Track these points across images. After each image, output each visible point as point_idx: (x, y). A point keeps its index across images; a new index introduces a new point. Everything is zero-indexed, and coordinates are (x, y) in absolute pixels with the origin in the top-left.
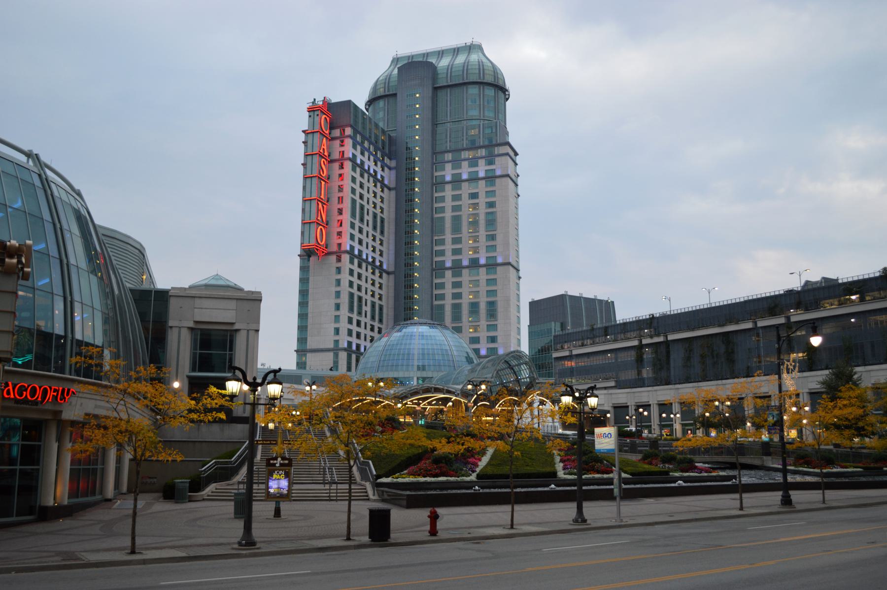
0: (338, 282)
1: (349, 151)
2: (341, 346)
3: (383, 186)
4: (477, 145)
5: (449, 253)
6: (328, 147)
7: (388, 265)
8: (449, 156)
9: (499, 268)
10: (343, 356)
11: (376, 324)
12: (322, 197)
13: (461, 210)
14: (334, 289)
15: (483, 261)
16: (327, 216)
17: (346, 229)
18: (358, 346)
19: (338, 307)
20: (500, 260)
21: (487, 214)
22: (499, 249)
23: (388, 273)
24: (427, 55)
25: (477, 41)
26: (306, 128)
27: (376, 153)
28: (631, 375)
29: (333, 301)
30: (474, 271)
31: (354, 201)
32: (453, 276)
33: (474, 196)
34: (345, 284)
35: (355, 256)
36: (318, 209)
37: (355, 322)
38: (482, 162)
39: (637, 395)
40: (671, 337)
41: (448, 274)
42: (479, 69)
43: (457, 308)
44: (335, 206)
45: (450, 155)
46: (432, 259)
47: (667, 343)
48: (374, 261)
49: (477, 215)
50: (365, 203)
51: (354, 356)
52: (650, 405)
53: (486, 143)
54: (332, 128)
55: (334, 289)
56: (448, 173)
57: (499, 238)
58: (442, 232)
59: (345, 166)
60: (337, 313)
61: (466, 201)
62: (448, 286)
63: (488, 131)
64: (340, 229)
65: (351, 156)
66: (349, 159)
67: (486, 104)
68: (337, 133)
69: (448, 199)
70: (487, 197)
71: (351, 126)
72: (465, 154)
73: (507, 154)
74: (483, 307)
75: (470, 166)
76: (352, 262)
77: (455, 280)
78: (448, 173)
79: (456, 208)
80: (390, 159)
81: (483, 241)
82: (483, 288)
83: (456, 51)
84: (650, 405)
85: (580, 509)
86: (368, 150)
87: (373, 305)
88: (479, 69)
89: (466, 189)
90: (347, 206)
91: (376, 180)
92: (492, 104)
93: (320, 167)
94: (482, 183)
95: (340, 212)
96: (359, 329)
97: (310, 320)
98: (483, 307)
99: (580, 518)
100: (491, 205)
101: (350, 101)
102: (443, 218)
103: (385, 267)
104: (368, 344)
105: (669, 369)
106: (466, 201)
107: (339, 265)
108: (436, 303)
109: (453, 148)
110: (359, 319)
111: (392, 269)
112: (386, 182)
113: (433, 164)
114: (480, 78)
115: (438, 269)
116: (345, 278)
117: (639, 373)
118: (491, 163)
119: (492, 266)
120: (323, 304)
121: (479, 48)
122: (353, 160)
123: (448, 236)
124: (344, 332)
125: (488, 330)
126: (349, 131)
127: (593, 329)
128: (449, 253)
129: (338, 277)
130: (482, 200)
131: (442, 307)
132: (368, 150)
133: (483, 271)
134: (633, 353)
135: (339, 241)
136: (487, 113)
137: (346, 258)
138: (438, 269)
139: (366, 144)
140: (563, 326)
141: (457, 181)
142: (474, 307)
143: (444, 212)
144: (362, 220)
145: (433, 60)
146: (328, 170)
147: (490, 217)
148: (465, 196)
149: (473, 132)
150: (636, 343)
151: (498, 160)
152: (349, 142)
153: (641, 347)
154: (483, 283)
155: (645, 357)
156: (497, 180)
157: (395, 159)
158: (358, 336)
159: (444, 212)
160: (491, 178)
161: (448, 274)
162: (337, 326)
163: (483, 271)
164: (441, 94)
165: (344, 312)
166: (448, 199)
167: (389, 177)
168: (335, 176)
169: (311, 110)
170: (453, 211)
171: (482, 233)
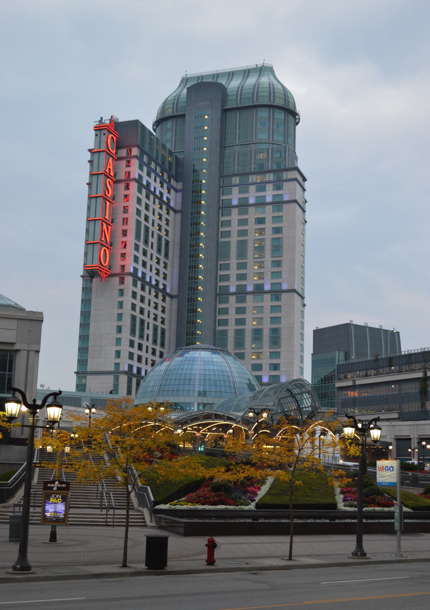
0: (121, 305)
2: (121, 369)
4: (265, 169)
8: (236, 180)
9: (285, 206)
10: (123, 379)
11: (158, 348)
14: (116, 311)
15: (267, 287)
17: (130, 251)
18: (139, 370)
19: (119, 329)
21: (274, 239)
22: (285, 275)
25: (268, 63)
29: (115, 324)
31: (138, 223)
33: (260, 221)
34: (127, 306)
35: (139, 278)
37: (136, 345)
38: (269, 187)
41: (232, 299)
43: (240, 334)
45: (238, 178)
50: (150, 225)
51: (134, 380)
53: (275, 167)
54: (118, 147)
55: (116, 311)
56: (235, 197)
58: (227, 256)
59: (130, 187)
60: (119, 336)
61: (252, 226)
63: (276, 155)
65: (137, 177)
66: (135, 180)
67: (275, 127)
68: (123, 153)
69: (235, 223)
70: (273, 222)
71: (138, 147)
72: (253, 179)
73: (296, 179)
74: (266, 333)
75: (258, 190)
76: (135, 285)
78: (235, 197)
80: (177, 181)
82: (267, 315)
83: (247, 73)
86: (155, 171)
87: (155, 328)
89: (253, 214)
90: (131, 227)
92: (282, 128)
94: (269, 208)
95: (125, 233)
96: (140, 353)
97: (91, 343)
98: (266, 333)
100: (278, 230)
101: (137, 121)
103: (168, 290)
104: (149, 368)
106: (252, 226)
108: (219, 328)
110: (141, 342)
111: (175, 293)
112: (172, 204)
115: (223, 294)
116: (128, 300)
120: (104, 325)
121: (270, 70)
122: (139, 181)
123: (233, 261)
124: (125, 355)
126: (135, 151)
127: (377, 360)
128: (233, 278)
129: (121, 299)
130: (269, 225)
131: (224, 333)
132: (155, 171)
133: (267, 297)
136: (276, 137)
137: (129, 280)
138: (223, 294)
139: (153, 165)
140: (347, 356)
141: (244, 206)
142: (257, 334)
147: (276, 243)
149: (261, 156)
150: (420, 375)
152: (135, 163)
157: (181, 181)
158: (139, 359)
160: (278, 203)
161: (232, 299)
162: (118, 348)
163: (267, 297)
164: (230, 116)
165: (126, 335)
166: (235, 223)
167: (175, 200)
171: (268, 259)
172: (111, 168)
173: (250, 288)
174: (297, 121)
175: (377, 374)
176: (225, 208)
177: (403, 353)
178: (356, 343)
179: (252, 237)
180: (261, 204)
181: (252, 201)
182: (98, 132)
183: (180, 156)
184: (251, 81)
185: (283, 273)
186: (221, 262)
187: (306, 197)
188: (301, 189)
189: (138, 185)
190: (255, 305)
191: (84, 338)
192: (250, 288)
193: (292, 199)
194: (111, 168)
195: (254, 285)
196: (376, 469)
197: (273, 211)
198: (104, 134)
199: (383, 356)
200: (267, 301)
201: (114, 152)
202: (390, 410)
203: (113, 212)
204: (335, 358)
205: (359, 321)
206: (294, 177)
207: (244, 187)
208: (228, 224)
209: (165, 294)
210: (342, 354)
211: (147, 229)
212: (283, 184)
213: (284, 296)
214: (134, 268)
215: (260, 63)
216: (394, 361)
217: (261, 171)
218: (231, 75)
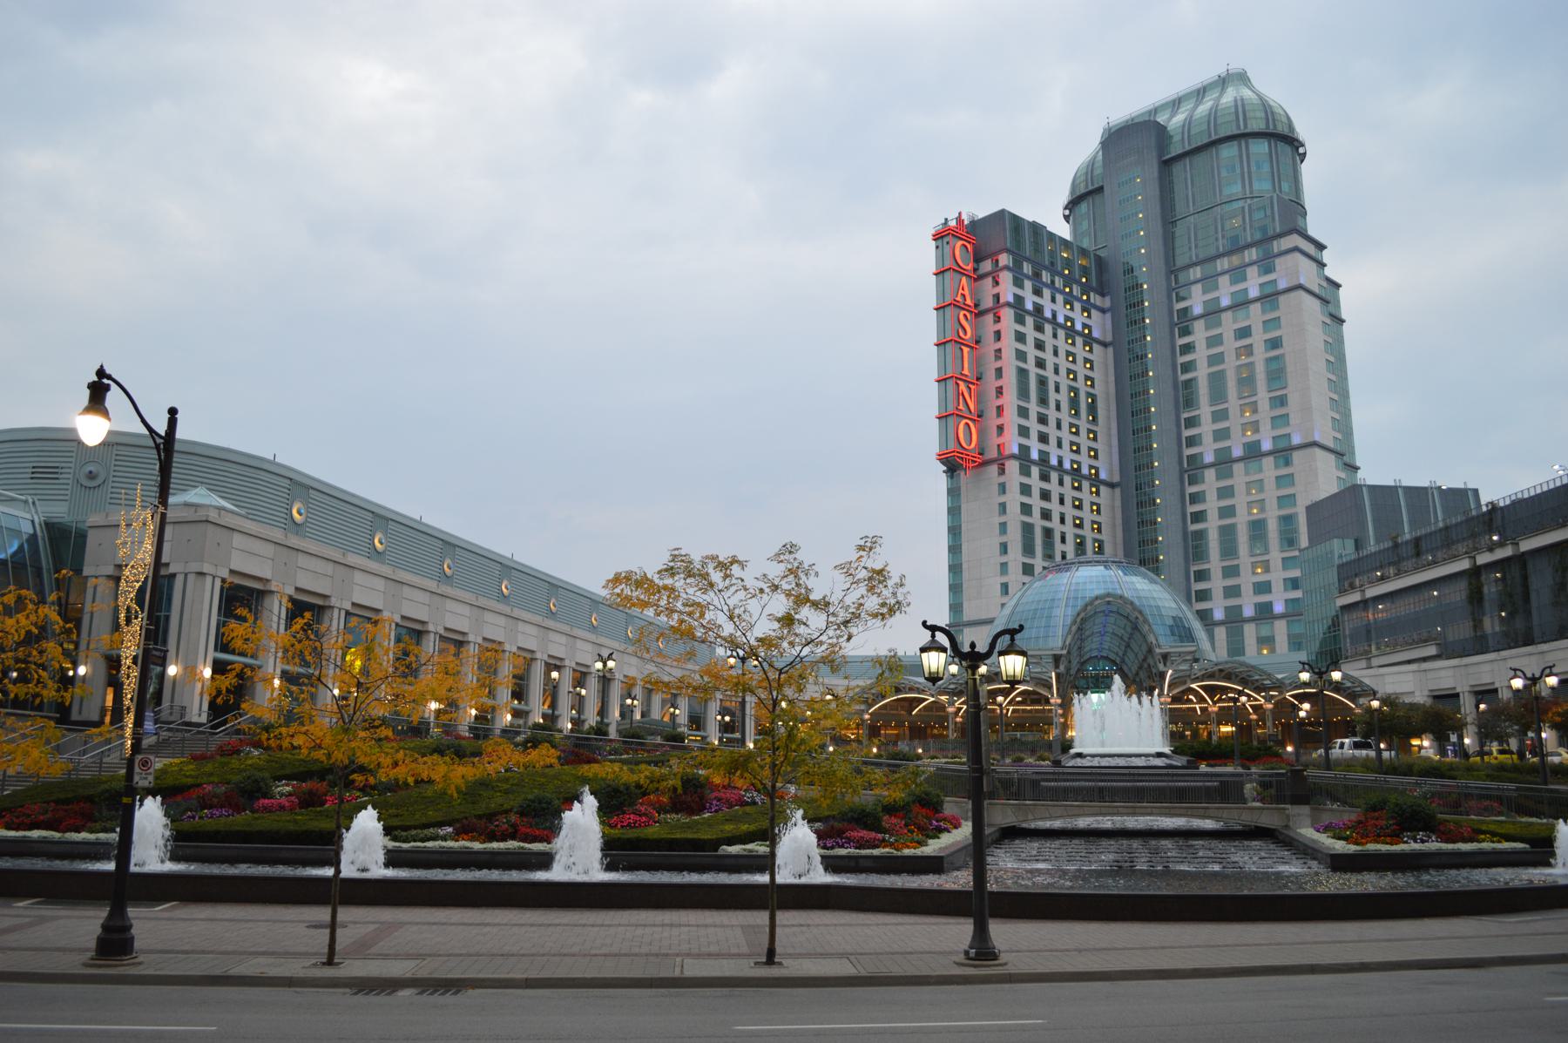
0: (1003, 508)
3: (1089, 340)
4: (1242, 243)
6: (973, 293)
7: (1111, 472)
8: (1196, 273)
12: (966, 372)
13: (1223, 361)
15: (1267, 446)
16: (978, 402)
17: (1011, 419)
19: (1004, 548)
21: (1269, 360)
23: (1112, 485)
24: (1156, 111)
25: (1235, 66)
27: (1053, 282)
28: (1461, 631)
30: (1253, 465)
32: (1219, 478)
33: (1244, 333)
34: (1014, 509)
36: (964, 394)
38: (1252, 272)
39: (1471, 670)
40: (1526, 545)
41: (1210, 474)
42: (1237, 113)
43: (1228, 533)
44: (991, 382)
47: (1521, 559)
48: (1060, 462)
49: (1251, 365)
52: (1457, 695)
53: (1258, 236)
54: (978, 259)
55: (998, 520)
60: (1004, 559)
61: (1230, 345)
63: (1259, 215)
64: (999, 421)
65: (1011, 299)
67: (1254, 169)
68: (987, 266)
69: (1201, 346)
70: (1265, 331)
71: (1007, 251)
72: (1223, 264)
74: (1273, 527)
75: (1234, 282)
77: (1223, 484)
79: (1216, 359)
80: (1103, 295)
81: (1265, 411)
82: (1271, 493)
83: (1200, 93)
84: (1457, 695)
85: (981, 933)
88: (1237, 113)
89: (1229, 324)
90: (1010, 381)
91: (1071, 333)
92: (1266, 168)
93: (963, 320)
94: (1256, 309)
95: (1000, 391)
97: (965, 575)
98: (1273, 527)
99: (983, 951)
100: (1275, 343)
101: (1003, 211)
103: (1103, 476)
105: (1528, 613)
106: (1230, 345)
107: (1002, 479)
108: (1194, 527)
109: (1201, 256)
112: (1096, 334)
113: (1170, 290)
114: (1238, 127)
115: (1192, 469)
116: (1014, 499)
117: (1477, 624)
118: (1269, 270)
119: (1283, 453)
120: (981, 546)
123: (1205, 410)
125: (1285, 568)
126: (1004, 259)
127: (1396, 545)
128: (1208, 439)
129: (1002, 499)
130: (1258, 339)
131: (1200, 535)
133: (1268, 462)
134: (1462, 586)
135: (1000, 441)
136: (1256, 186)
137: (1013, 467)
138: (1192, 469)
139: (1046, 277)
140: (1358, 545)
141: (1213, 313)
142: (1257, 528)
144: (1043, 401)
145: (1161, 119)
146: (975, 328)
147: (1274, 366)
148: (1228, 336)
149: (1236, 222)
150: (1464, 565)
152: (1006, 278)
153: (1476, 572)
154: (1270, 483)
155: (1486, 590)
156: (1282, 298)
160: (1270, 297)
161: (1210, 474)
162: (1004, 579)
163: (1268, 462)
164: (1177, 169)
167: (1100, 325)
168: (989, 337)
169: (938, 237)
171: (1263, 396)
172: (966, 292)
173: (1237, 452)
175: (1399, 574)
176: (1183, 323)
178: (1374, 521)
179: (1230, 365)
180: (1241, 303)
181: (1225, 302)
183: (1101, 253)
184: (1204, 108)
185: (1291, 416)
186: (1186, 415)
188: (1314, 265)
190: (1248, 479)
191: (955, 569)
192: (1237, 452)
194: (966, 292)
197: (1264, 312)
199: (1407, 537)
200: (1268, 466)
201: (969, 268)
202: (1425, 641)
203: (977, 362)
204: (1332, 552)
206: (1291, 246)
207: (1209, 281)
208: (1188, 348)
209: (1095, 481)
210: (1350, 544)
213: (1297, 456)
214: (1021, 446)
215: (1222, 71)
216: (1423, 546)
217: (1237, 248)
218: (1176, 104)
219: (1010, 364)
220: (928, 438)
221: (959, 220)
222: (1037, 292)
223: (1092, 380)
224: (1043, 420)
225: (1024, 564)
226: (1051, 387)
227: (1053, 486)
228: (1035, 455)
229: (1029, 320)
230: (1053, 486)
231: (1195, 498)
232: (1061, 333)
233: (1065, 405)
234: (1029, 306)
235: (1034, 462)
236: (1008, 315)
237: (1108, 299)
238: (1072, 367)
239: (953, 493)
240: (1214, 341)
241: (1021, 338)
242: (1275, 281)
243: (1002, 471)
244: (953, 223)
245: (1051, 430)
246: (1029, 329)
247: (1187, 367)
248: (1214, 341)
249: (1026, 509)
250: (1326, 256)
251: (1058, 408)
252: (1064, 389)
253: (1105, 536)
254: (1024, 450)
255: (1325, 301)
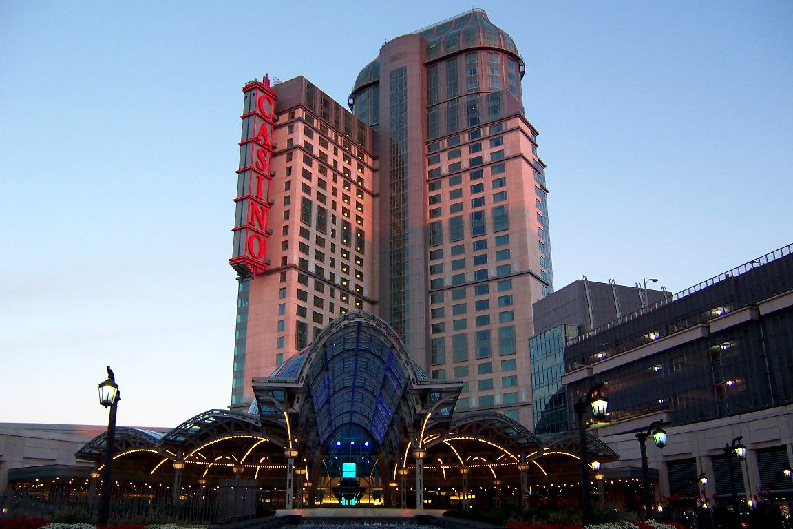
1: (300, 138)
5: (448, 268)
9: (507, 164)
13: (465, 312)
17: (296, 238)
20: (516, 269)
21: (501, 329)
22: (514, 254)
26: (230, 405)
27: (336, 139)
29: (275, 336)
32: (455, 298)
41: (448, 295)
45: (446, 141)
46: (426, 277)
55: (277, 319)
56: (444, 166)
57: (514, 239)
62: (449, 312)
65: (301, 143)
68: (285, 118)
73: (519, 129)
91: (345, 291)
95: (287, 215)
101: (301, 78)
102: (443, 339)
103: (366, 294)
107: (283, 285)
116: (293, 302)
119: (505, 278)
123: (446, 247)
126: (300, 113)
128: (448, 268)
138: (434, 291)
141: (455, 174)
143: (441, 271)
148: (466, 190)
151: (507, 138)
152: (300, 127)
159: (441, 271)
161: (448, 295)
170: (453, 255)
174: (522, 69)
177: (675, 298)
182: (248, 94)
187: (542, 154)
189: (304, 155)
193: (515, 153)
195: (475, 272)
196: (745, 492)
198: (254, 94)
205: (599, 276)
206: (514, 126)
211: (322, 211)
212: (502, 137)
213: (516, 282)
219: (298, 195)
220: (225, 246)
221: (266, 79)
222: (323, 144)
223: (361, 219)
224: (320, 242)
225: (298, 322)
226: (330, 218)
227: (325, 296)
228: (312, 269)
229: (315, 163)
230: (325, 296)
231: (434, 256)
232: (337, 293)
233: (339, 234)
234: (316, 152)
235: (311, 274)
236: (299, 155)
237: (377, 162)
238: (345, 262)
239: (243, 296)
240: (456, 194)
241: (307, 175)
242: (502, 151)
243: (284, 279)
244: (260, 80)
245: (326, 250)
246: (314, 169)
247: (434, 213)
248: (456, 194)
249: (301, 311)
250: (538, 140)
251: (333, 236)
252: (339, 221)
253: (367, 228)
254: (304, 263)
255: (537, 171)
